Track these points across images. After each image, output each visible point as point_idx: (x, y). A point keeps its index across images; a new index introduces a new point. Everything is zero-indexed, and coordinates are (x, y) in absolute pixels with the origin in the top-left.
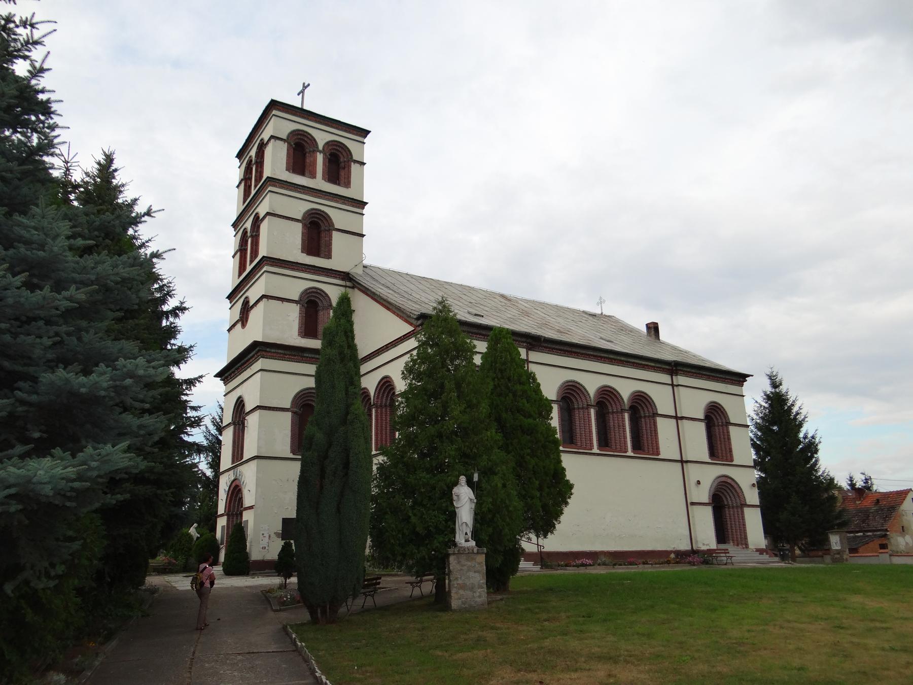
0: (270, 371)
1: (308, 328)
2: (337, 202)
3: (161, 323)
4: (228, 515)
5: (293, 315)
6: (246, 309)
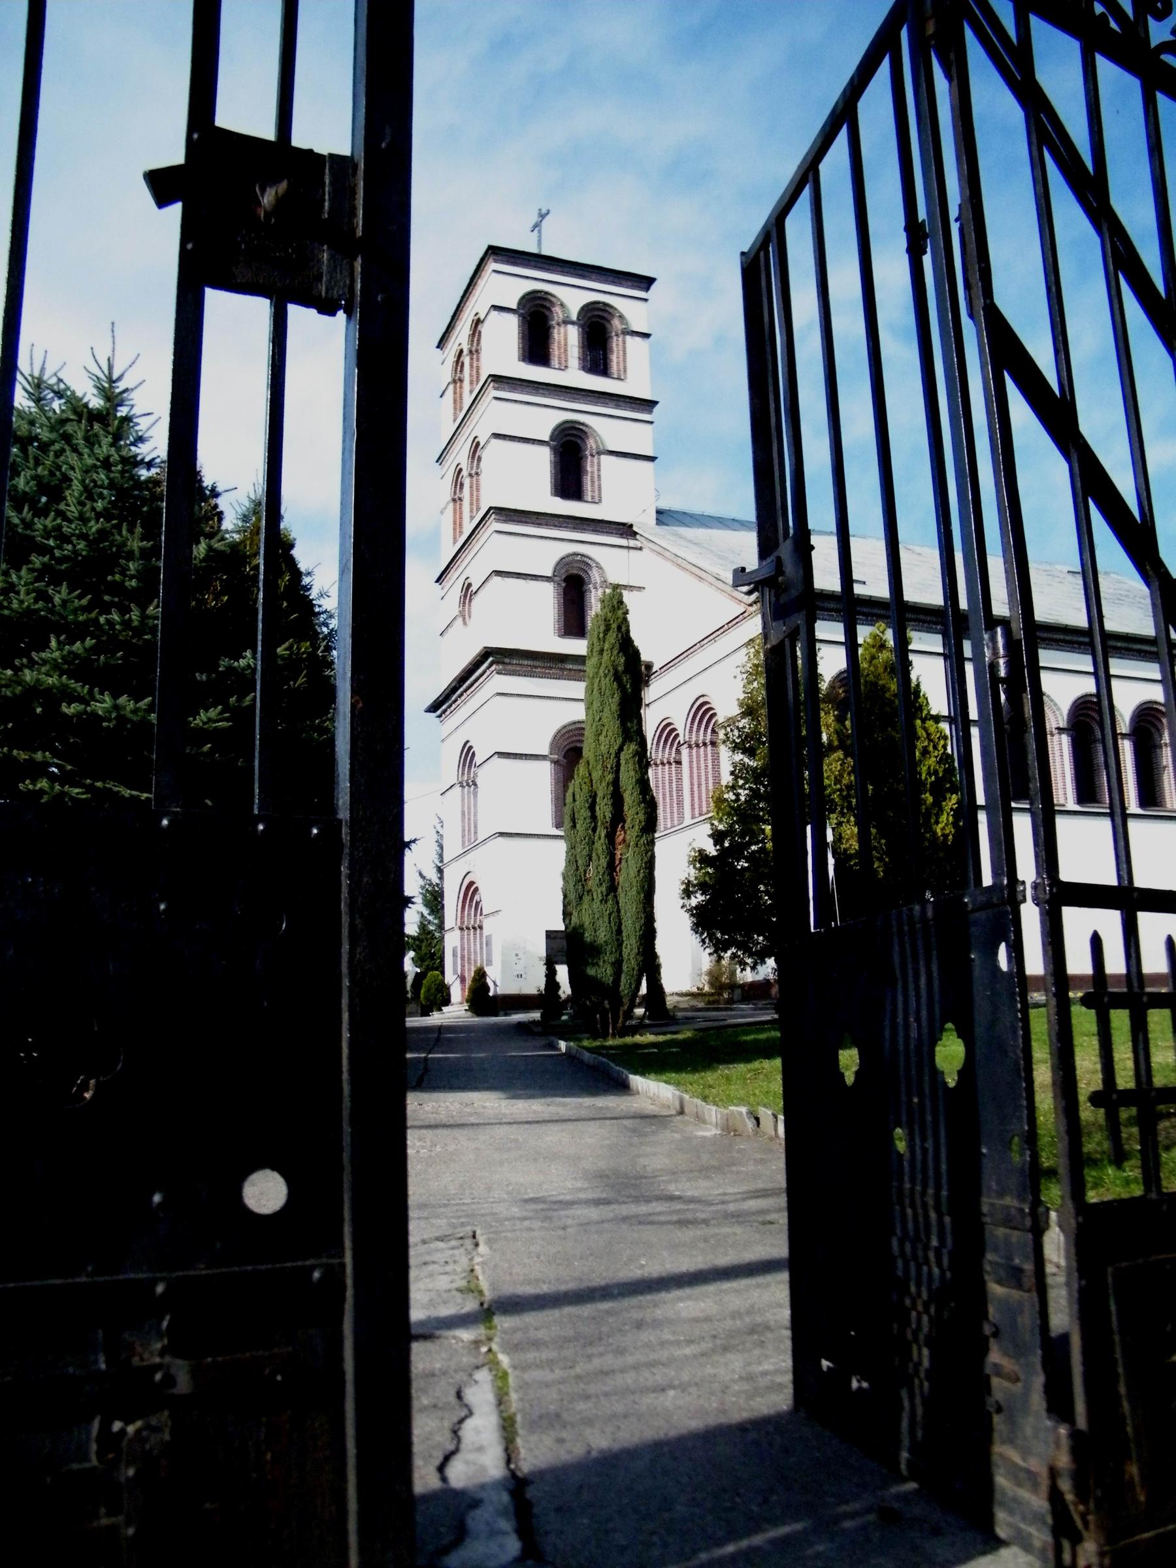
0: (512, 695)
1: (573, 620)
2: (605, 405)
3: (827, 1359)
4: (461, 929)
5: (545, 601)
6: (468, 593)
